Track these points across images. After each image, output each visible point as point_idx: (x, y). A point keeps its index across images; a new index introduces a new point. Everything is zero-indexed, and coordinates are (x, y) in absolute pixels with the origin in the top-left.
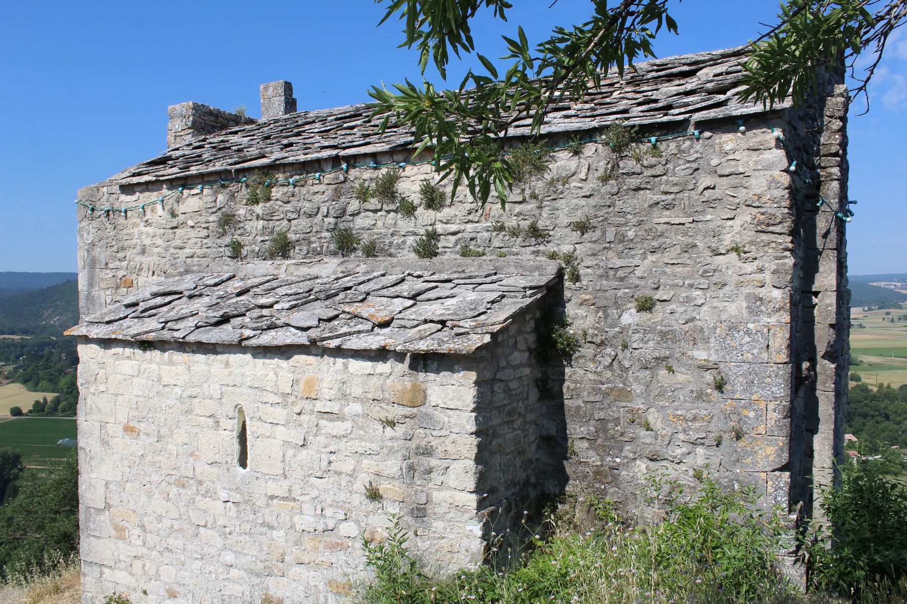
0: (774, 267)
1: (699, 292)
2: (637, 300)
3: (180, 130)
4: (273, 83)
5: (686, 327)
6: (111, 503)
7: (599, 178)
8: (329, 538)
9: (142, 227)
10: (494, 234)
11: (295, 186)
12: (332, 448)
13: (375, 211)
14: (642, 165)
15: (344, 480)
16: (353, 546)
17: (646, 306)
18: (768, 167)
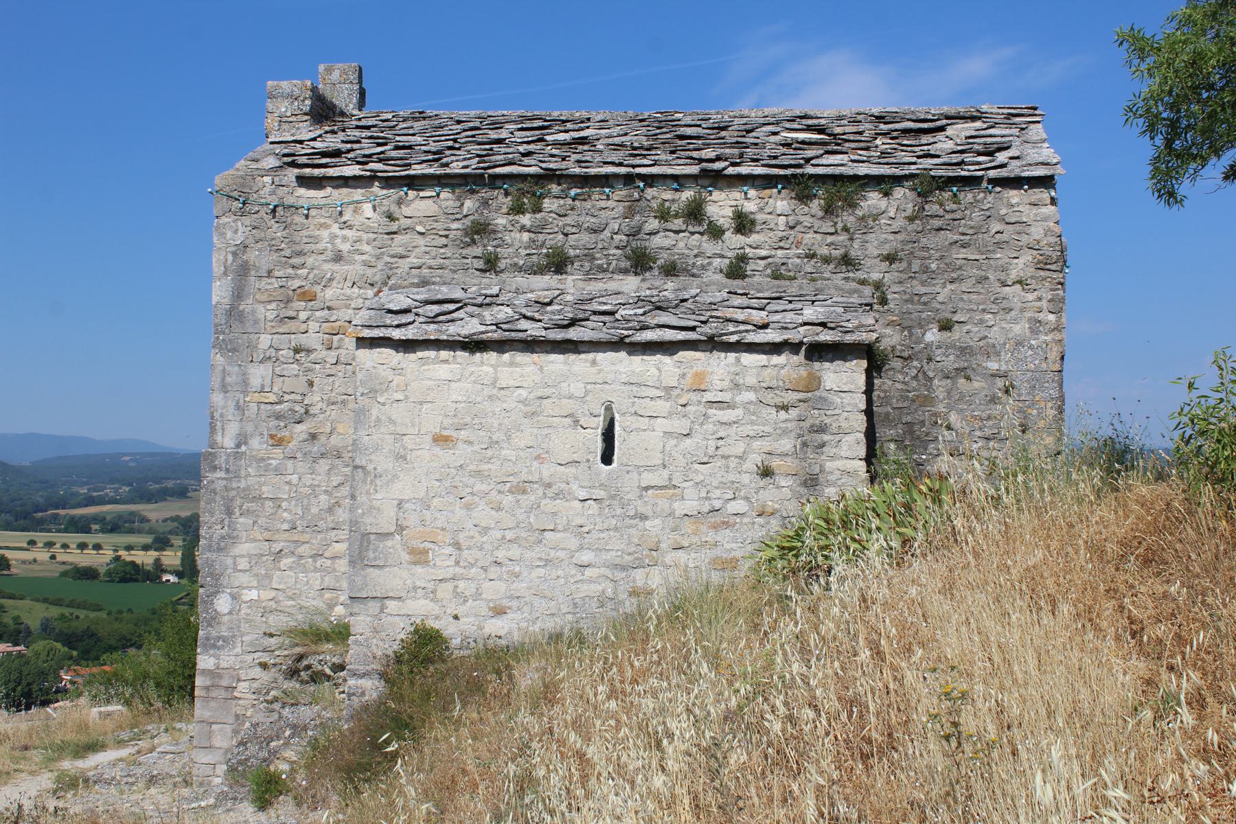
0: (1050, 297)
1: (990, 316)
2: (939, 322)
3: (289, 114)
4: (340, 65)
5: (981, 344)
6: (405, 523)
7: (906, 218)
8: (717, 518)
9: (335, 228)
10: (806, 260)
11: (574, 200)
12: (720, 435)
13: (677, 232)
14: (945, 210)
15: (733, 463)
16: (741, 522)
17: (946, 326)
18: (1045, 219)
